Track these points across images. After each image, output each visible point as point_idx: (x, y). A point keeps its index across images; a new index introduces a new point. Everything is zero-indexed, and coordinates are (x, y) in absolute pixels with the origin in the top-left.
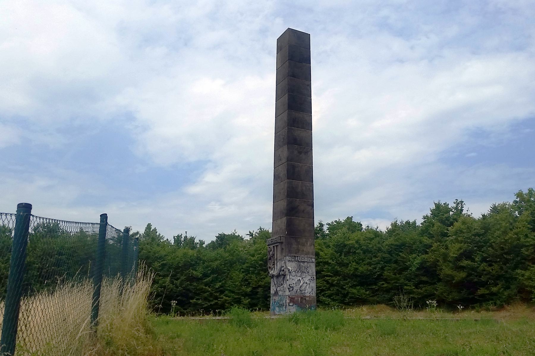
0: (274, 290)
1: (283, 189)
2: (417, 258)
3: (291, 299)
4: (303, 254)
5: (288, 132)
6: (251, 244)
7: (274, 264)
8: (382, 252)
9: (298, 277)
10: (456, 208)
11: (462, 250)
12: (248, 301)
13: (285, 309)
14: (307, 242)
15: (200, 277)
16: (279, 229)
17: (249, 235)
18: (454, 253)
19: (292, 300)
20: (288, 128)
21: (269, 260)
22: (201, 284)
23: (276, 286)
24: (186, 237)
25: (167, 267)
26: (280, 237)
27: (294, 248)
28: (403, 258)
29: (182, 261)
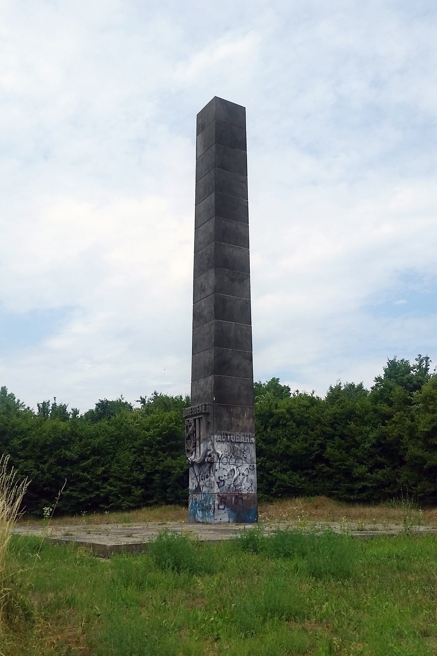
0: (194, 485)
1: (208, 334)
3: (222, 499)
4: (238, 432)
5: (215, 249)
6: (143, 414)
7: (196, 445)
8: (322, 424)
9: (230, 465)
10: (419, 367)
12: (141, 491)
13: (212, 514)
14: (243, 413)
15: (76, 459)
16: (202, 393)
17: (140, 401)
18: (424, 427)
19: (223, 500)
20: (215, 243)
21: (187, 439)
22: (77, 469)
24: (55, 404)
25: (30, 446)
26: (205, 405)
27: (225, 421)
29: (51, 437)
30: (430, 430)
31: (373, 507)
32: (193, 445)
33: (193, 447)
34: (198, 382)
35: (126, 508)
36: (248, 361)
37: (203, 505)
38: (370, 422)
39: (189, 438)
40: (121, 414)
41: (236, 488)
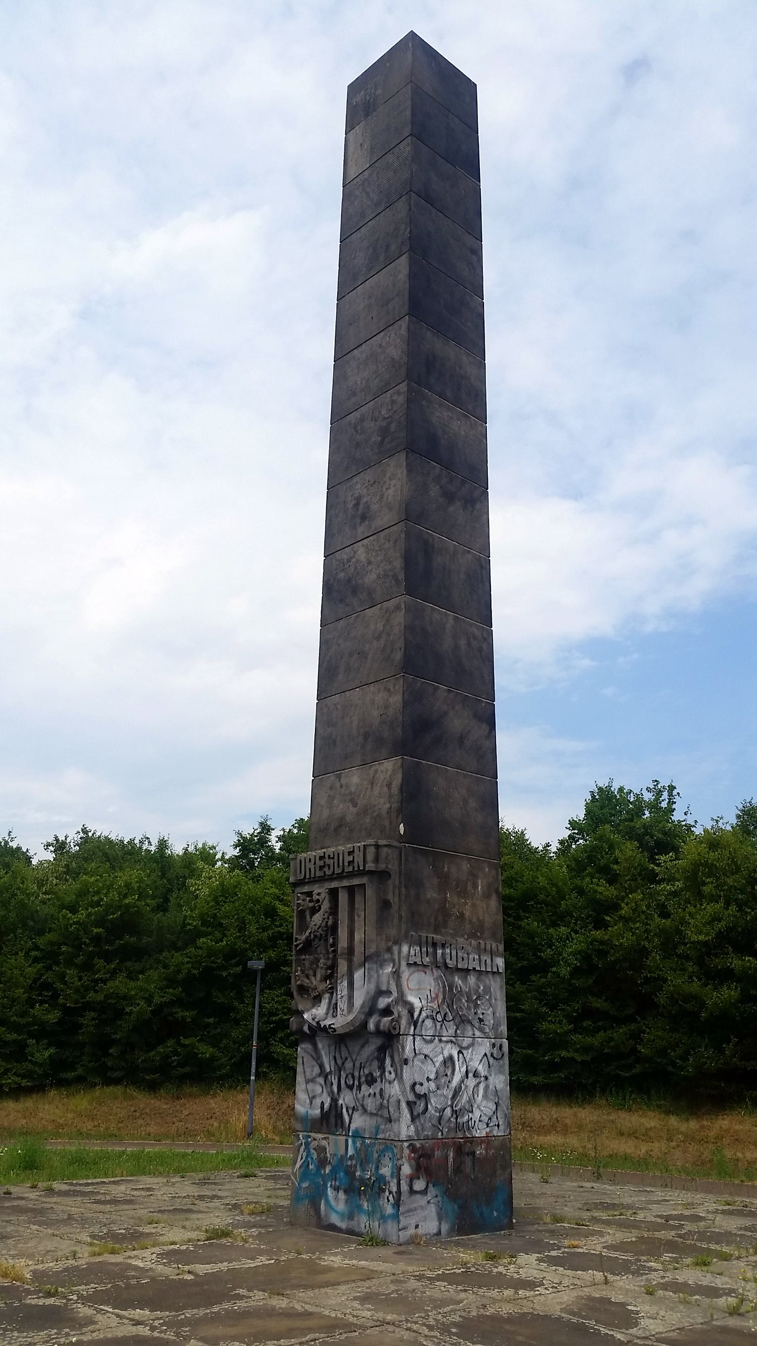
0: (318, 1102)
2: (572, 939)
3: (420, 1157)
9: (443, 1045)
11: (723, 923)
13: (389, 1210)
14: (473, 875)
16: (354, 810)
23: (327, 1083)
26: (377, 846)
27: (428, 902)
28: (531, 936)
30: (712, 940)
31: (580, 1106)
32: (323, 971)
33: (325, 978)
34: (339, 777)
35: (10, 1089)
36: (485, 727)
37: (350, 1173)
38: (572, 916)
39: (308, 946)
40: (12, 871)
41: (457, 1119)
